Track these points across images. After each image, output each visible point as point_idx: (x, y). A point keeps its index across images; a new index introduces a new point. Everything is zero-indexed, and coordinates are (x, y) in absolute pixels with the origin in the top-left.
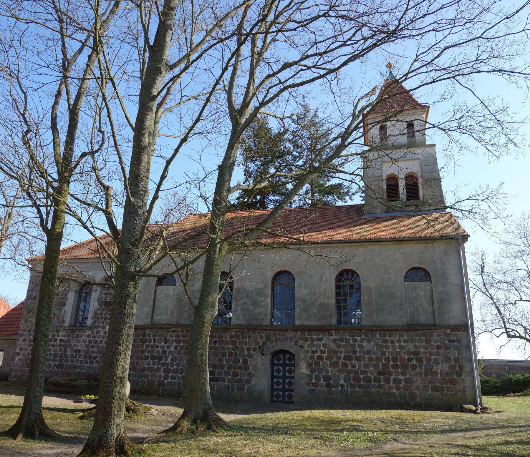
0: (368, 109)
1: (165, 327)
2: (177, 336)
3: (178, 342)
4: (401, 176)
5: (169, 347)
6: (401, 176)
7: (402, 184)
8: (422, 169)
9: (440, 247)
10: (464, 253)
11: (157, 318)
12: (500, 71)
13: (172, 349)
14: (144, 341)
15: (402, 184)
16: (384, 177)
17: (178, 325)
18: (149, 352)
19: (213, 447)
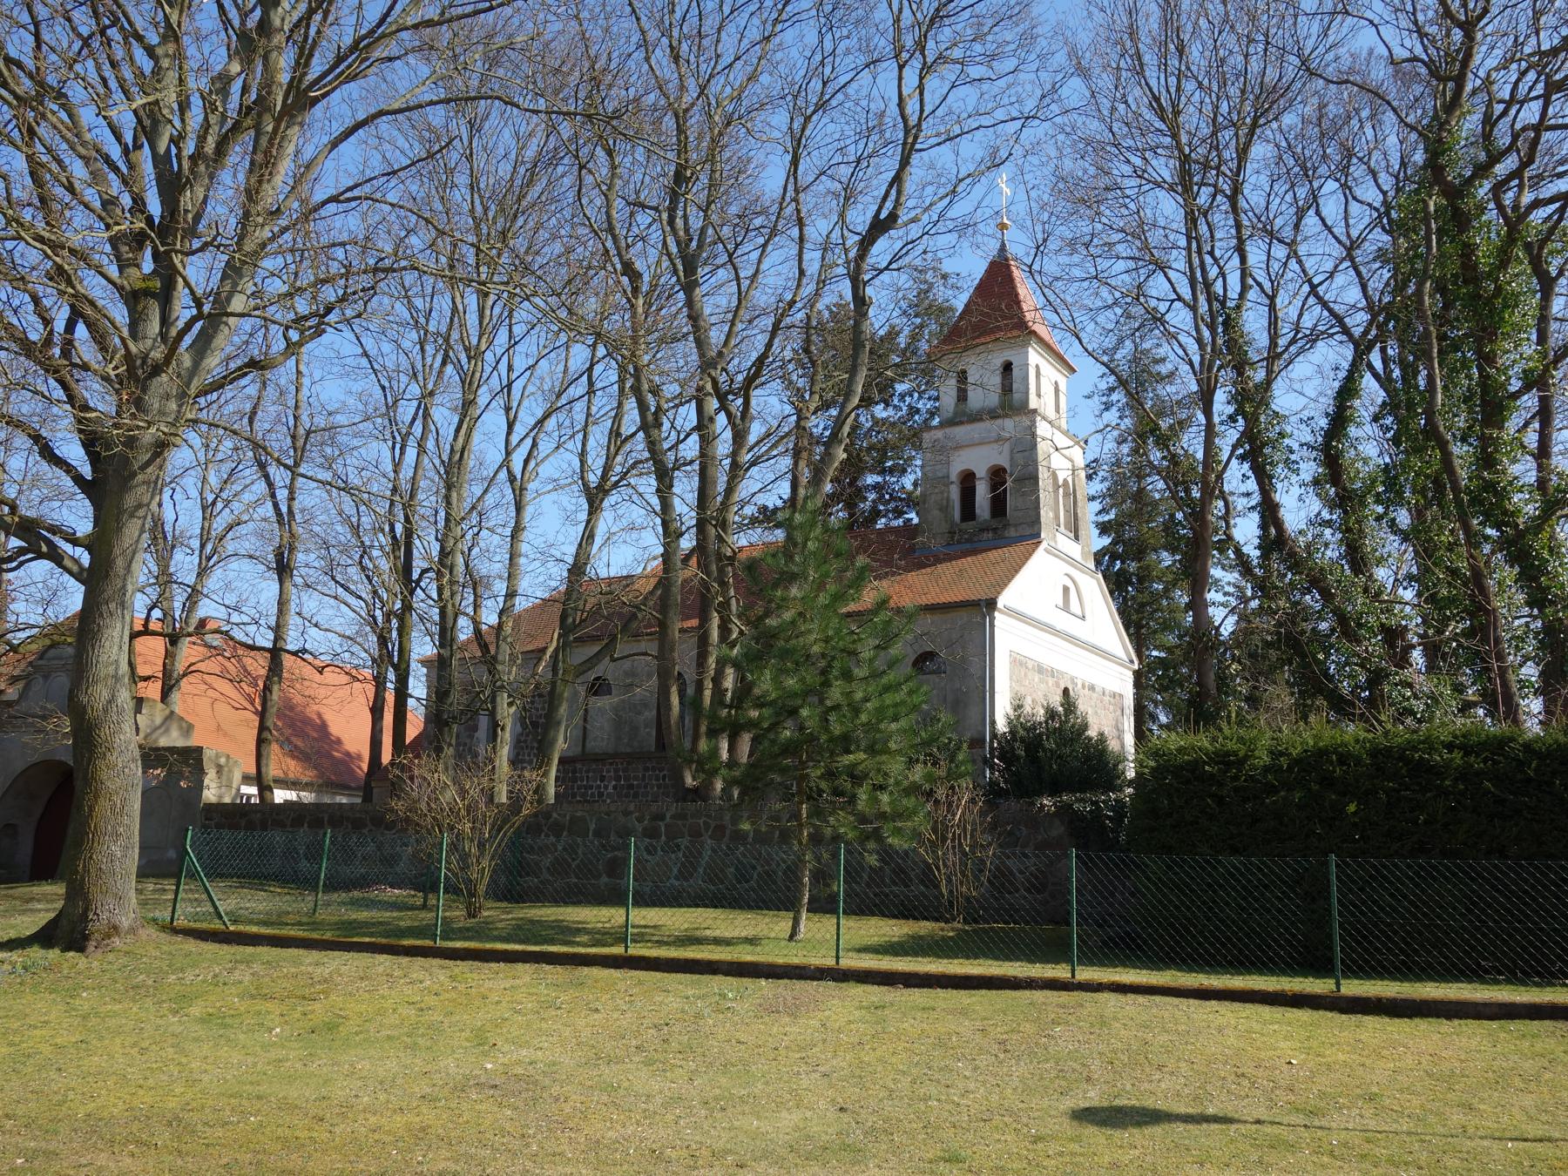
0: (28, 633)
1: (599, 759)
2: (616, 771)
3: (618, 779)
4: (981, 471)
5: (606, 787)
6: (981, 471)
7: (982, 492)
8: (1012, 459)
9: (962, 617)
10: (992, 626)
11: (590, 745)
12: (251, 557)
13: (610, 790)
14: (574, 780)
15: (982, 492)
16: (954, 477)
17: (615, 755)
18: (583, 795)
19: (204, 80)
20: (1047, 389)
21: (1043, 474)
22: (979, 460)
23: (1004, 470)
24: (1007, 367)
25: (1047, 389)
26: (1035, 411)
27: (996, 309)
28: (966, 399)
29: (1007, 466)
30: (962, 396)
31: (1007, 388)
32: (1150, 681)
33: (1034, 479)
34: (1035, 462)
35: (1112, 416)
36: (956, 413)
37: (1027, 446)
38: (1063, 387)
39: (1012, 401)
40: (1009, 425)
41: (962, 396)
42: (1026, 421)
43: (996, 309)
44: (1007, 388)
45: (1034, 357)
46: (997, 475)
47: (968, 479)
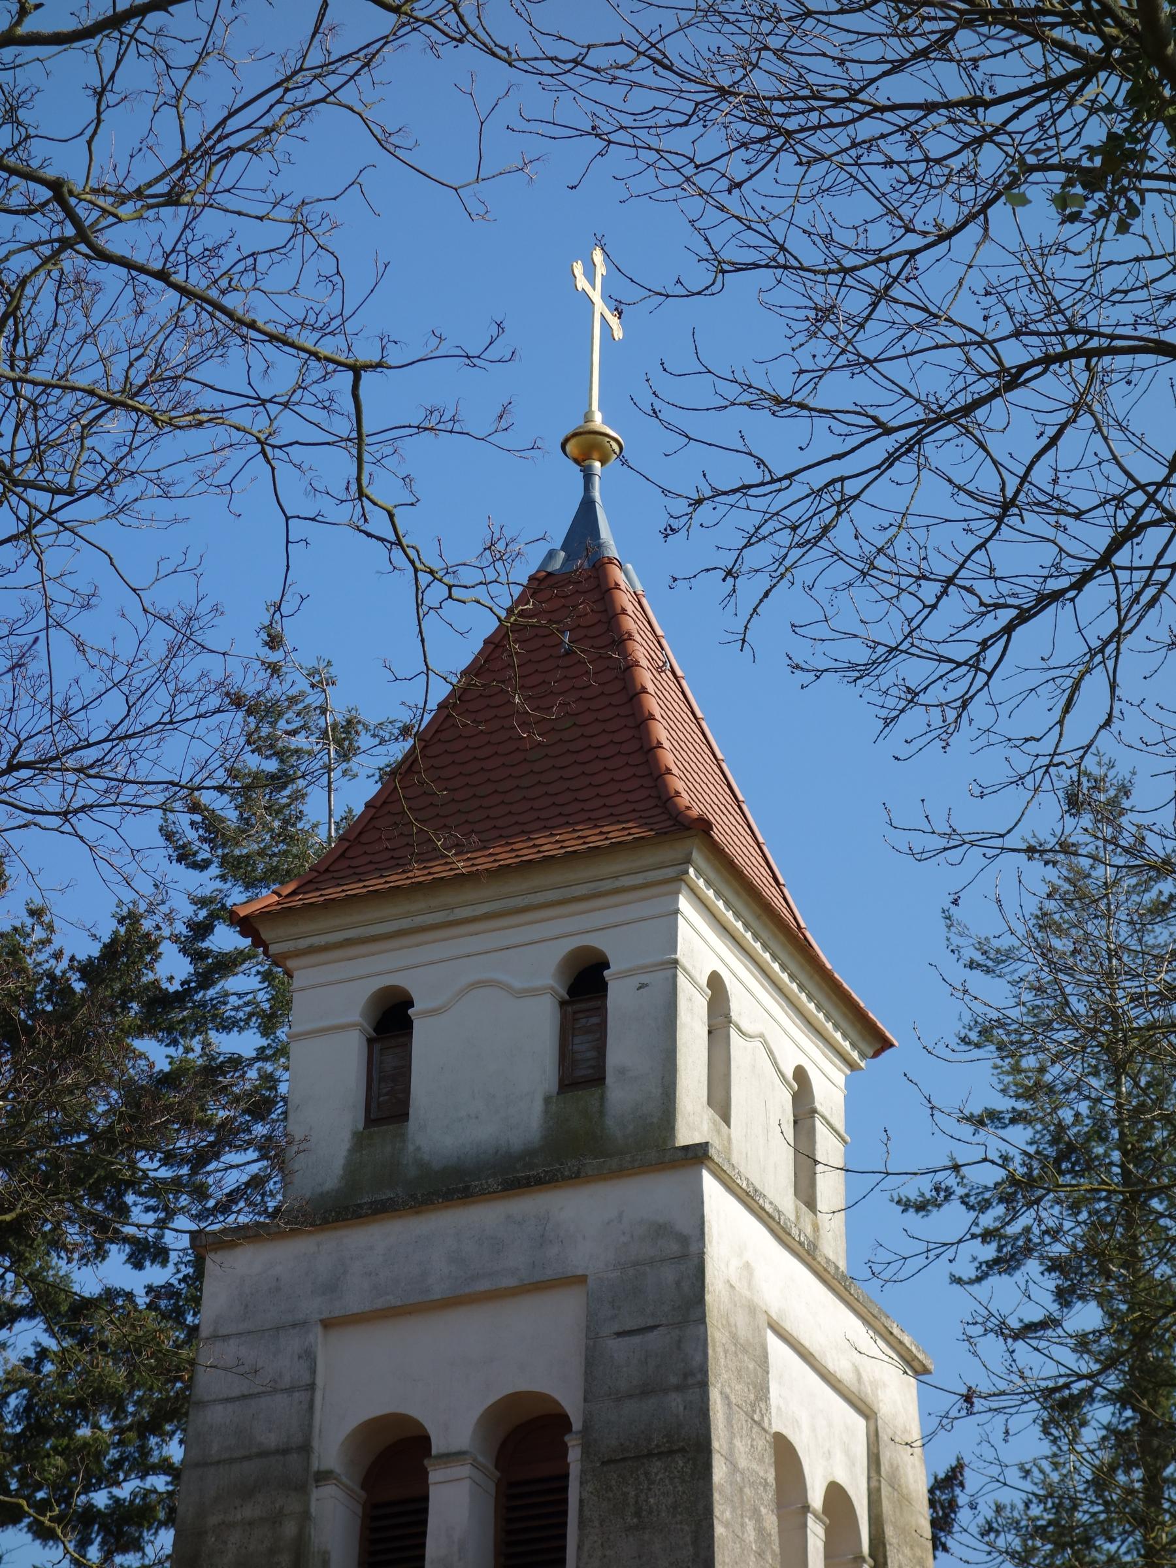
4: (456, 1427)
6: (456, 1427)
16: (331, 1448)
20: (760, 1104)
21: (735, 1461)
22: (447, 1377)
23: (561, 1422)
24: (586, 981)
25: (760, 1104)
26: (698, 1155)
27: (548, 752)
28: (402, 1115)
29: (572, 1405)
30: (387, 1098)
31: (581, 1066)
32: (165, 1474)
33: (694, 1450)
34: (695, 1380)
35: (1028, 1292)
36: (352, 1169)
37: (667, 1295)
38: (830, 1089)
39: (605, 1122)
40: (588, 1218)
41: (387, 1098)
42: (639, 1197)
43: (548, 752)
44: (581, 1066)
45: (702, 942)
46: (527, 1442)
47: (396, 1459)
